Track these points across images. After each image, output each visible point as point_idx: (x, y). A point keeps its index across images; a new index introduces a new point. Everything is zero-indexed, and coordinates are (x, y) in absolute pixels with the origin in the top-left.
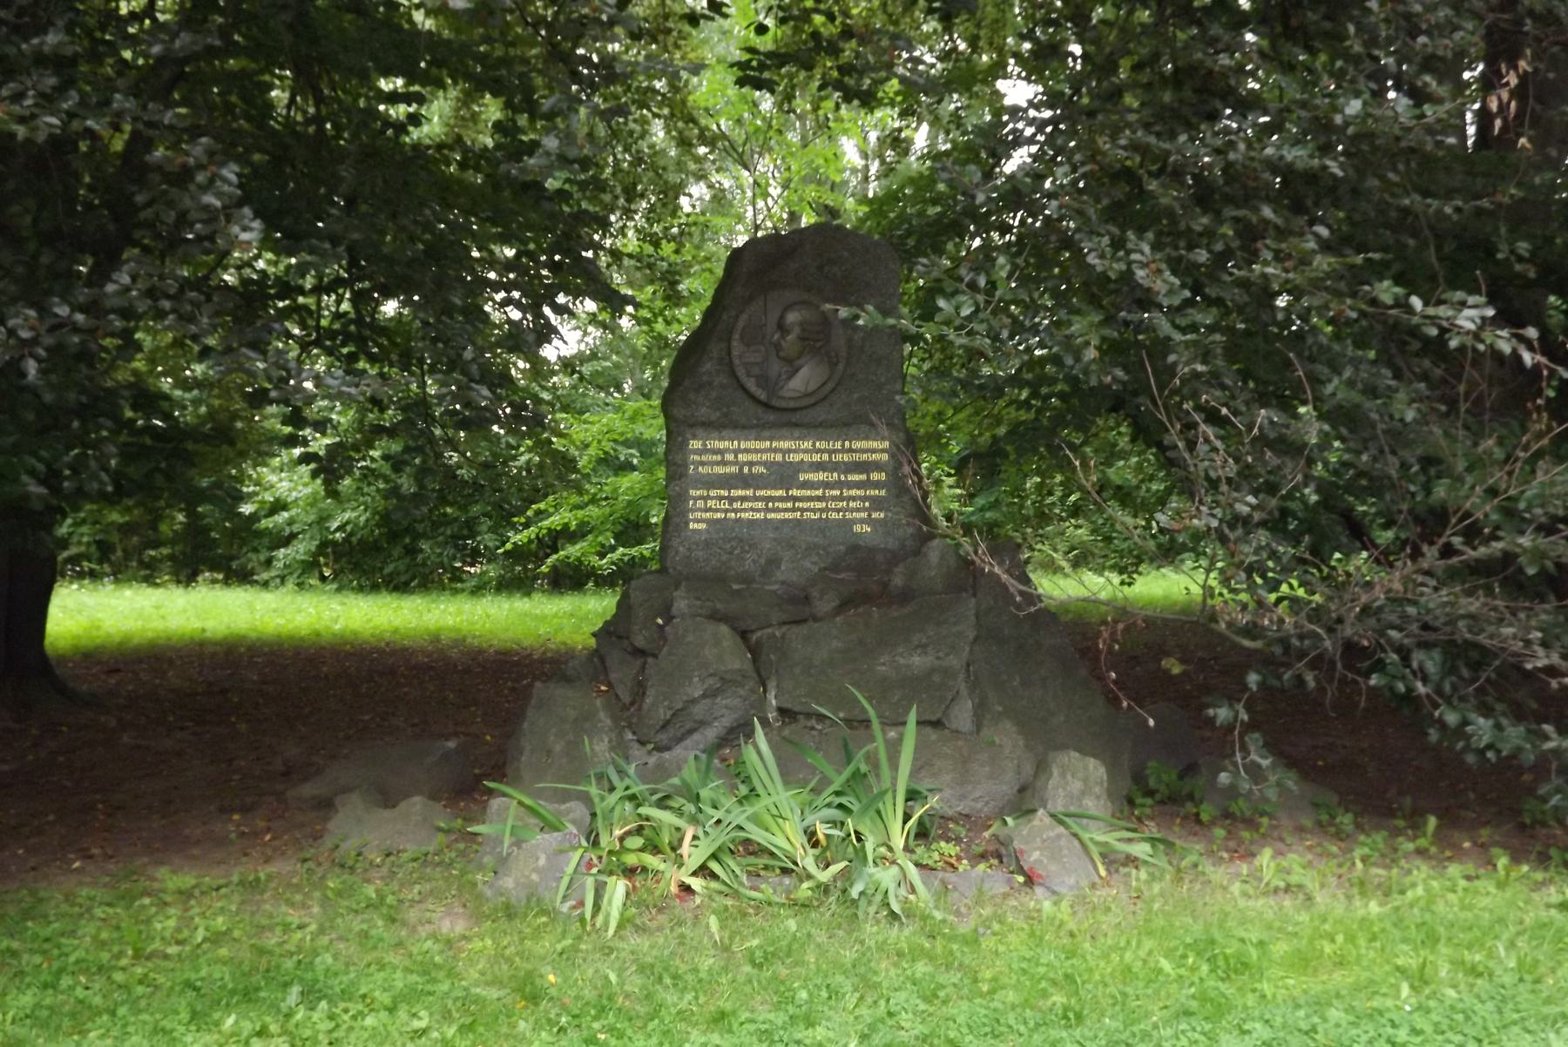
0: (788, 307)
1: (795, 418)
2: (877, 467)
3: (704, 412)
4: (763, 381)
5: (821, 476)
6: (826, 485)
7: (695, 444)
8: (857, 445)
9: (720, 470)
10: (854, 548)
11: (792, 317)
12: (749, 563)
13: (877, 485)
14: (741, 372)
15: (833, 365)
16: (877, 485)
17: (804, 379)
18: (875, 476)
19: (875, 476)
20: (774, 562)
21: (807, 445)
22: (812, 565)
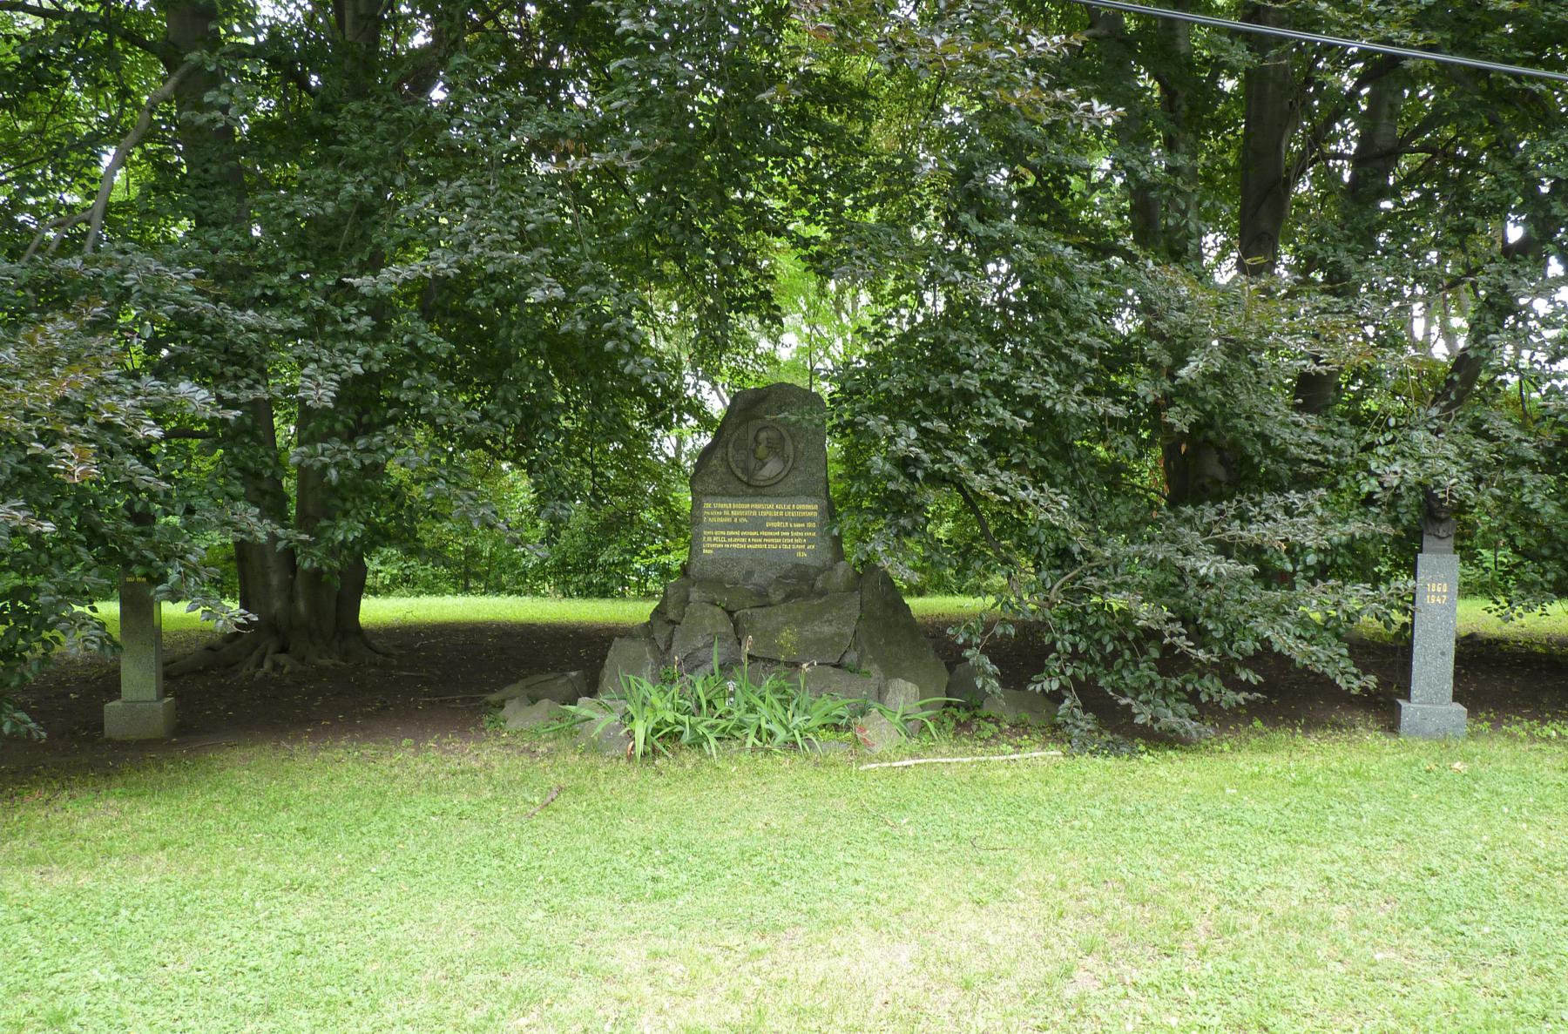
0: (760, 430)
1: (765, 491)
2: (811, 519)
3: (712, 487)
4: (745, 470)
5: (779, 524)
6: (782, 529)
7: (707, 505)
8: (799, 507)
9: (721, 520)
10: (796, 566)
11: (763, 435)
12: (736, 573)
13: (811, 530)
14: (733, 465)
15: (785, 462)
16: (811, 530)
17: (772, 468)
18: (810, 525)
19: (810, 525)
20: (750, 574)
21: (771, 506)
22: (772, 575)
